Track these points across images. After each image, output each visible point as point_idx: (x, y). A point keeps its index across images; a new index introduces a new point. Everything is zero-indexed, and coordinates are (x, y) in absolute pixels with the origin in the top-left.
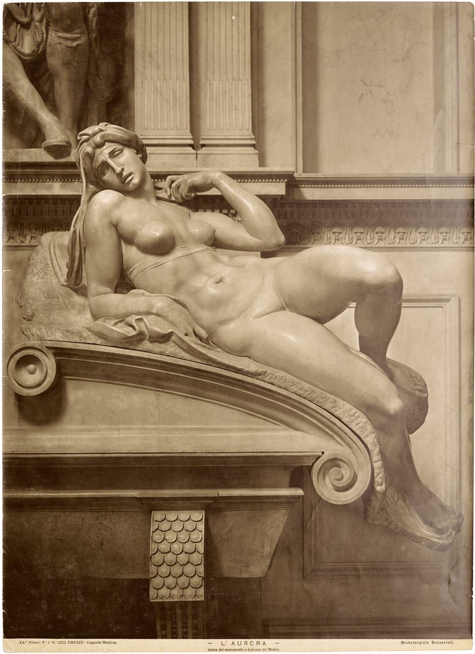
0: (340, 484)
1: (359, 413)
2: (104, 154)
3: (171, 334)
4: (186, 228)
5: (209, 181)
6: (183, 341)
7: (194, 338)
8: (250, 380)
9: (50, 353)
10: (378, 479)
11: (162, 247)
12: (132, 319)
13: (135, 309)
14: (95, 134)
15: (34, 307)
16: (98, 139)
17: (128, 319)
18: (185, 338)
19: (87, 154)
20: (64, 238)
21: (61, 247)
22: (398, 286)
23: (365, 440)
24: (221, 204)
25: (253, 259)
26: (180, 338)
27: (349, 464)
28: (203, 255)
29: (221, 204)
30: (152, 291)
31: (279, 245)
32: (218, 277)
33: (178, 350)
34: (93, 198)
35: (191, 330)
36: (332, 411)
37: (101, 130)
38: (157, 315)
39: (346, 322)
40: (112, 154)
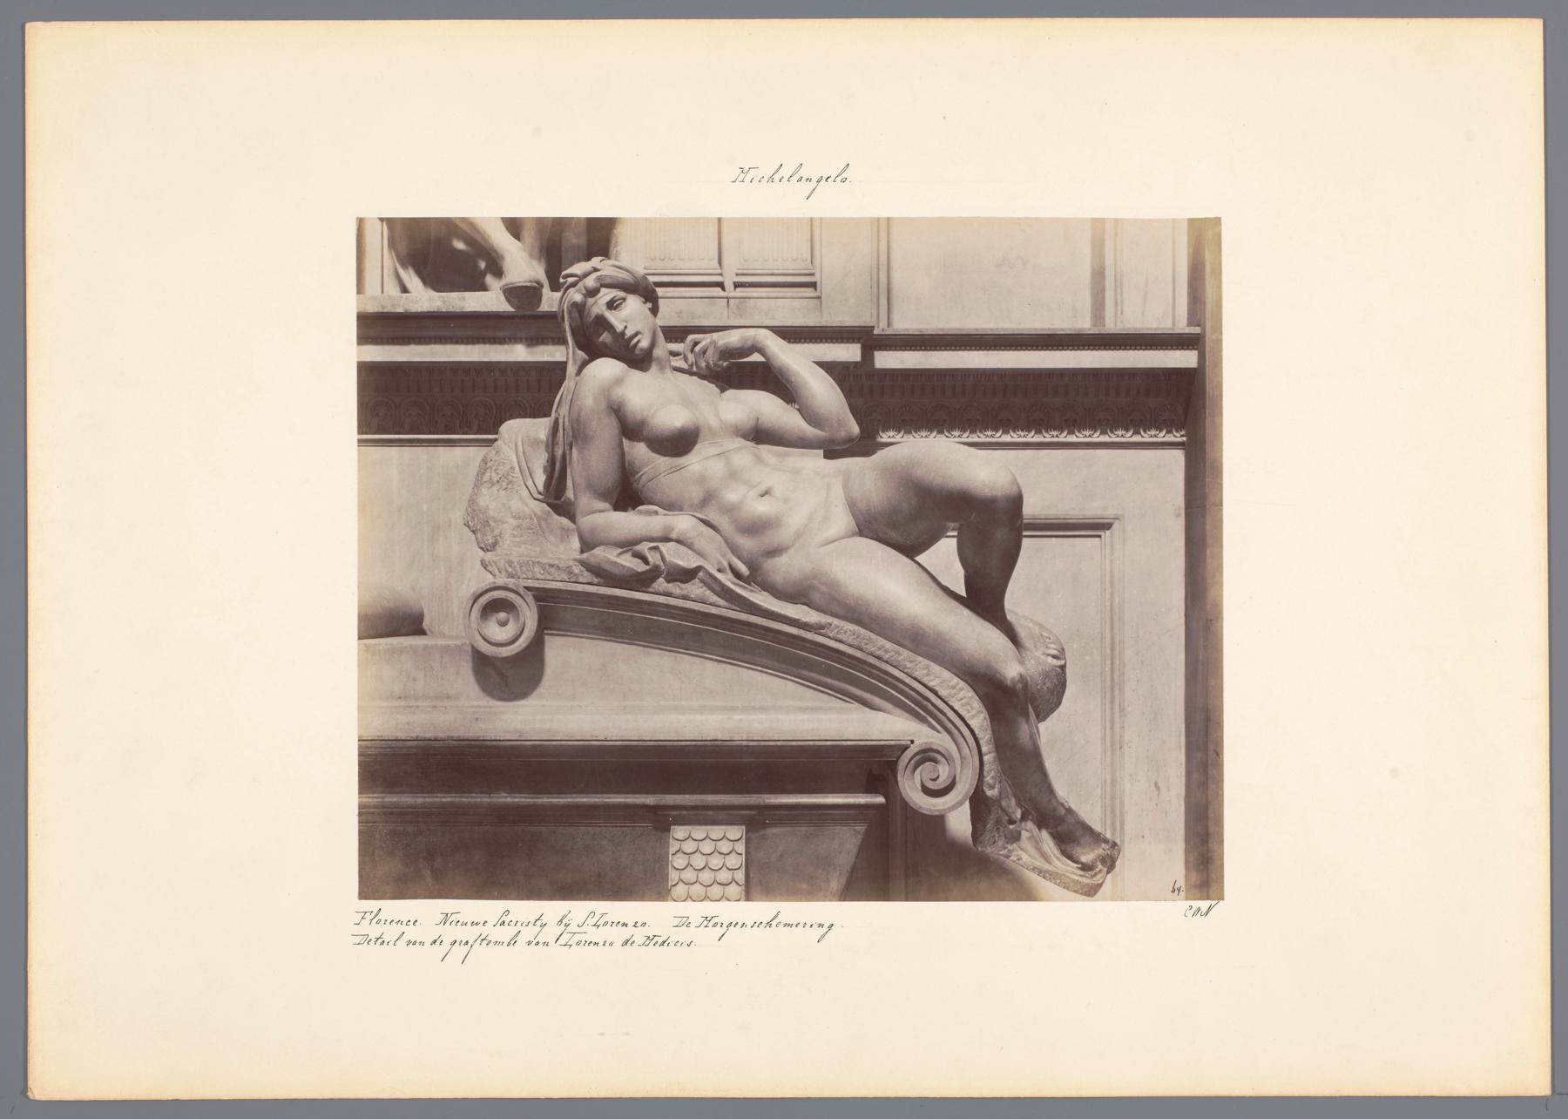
0: (930, 785)
1: (962, 684)
2: (599, 305)
3: (699, 568)
4: (717, 415)
5: (749, 343)
6: (715, 579)
7: (731, 576)
8: (809, 636)
9: (530, 597)
10: (988, 779)
11: (680, 443)
12: (644, 548)
13: (646, 533)
14: (586, 275)
15: (497, 532)
16: (590, 282)
17: (638, 548)
18: (719, 576)
19: (575, 305)
20: (539, 428)
21: (535, 443)
22: (1017, 501)
23: (972, 723)
24: (769, 378)
25: (813, 461)
26: (711, 575)
27: (948, 759)
28: (744, 455)
29: (769, 378)
30: (671, 507)
31: (850, 440)
32: (763, 487)
33: (708, 593)
34: (585, 371)
35: (725, 564)
36: (925, 680)
37: (596, 270)
38: (678, 541)
39: (945, 556)
40: (612, 305)
